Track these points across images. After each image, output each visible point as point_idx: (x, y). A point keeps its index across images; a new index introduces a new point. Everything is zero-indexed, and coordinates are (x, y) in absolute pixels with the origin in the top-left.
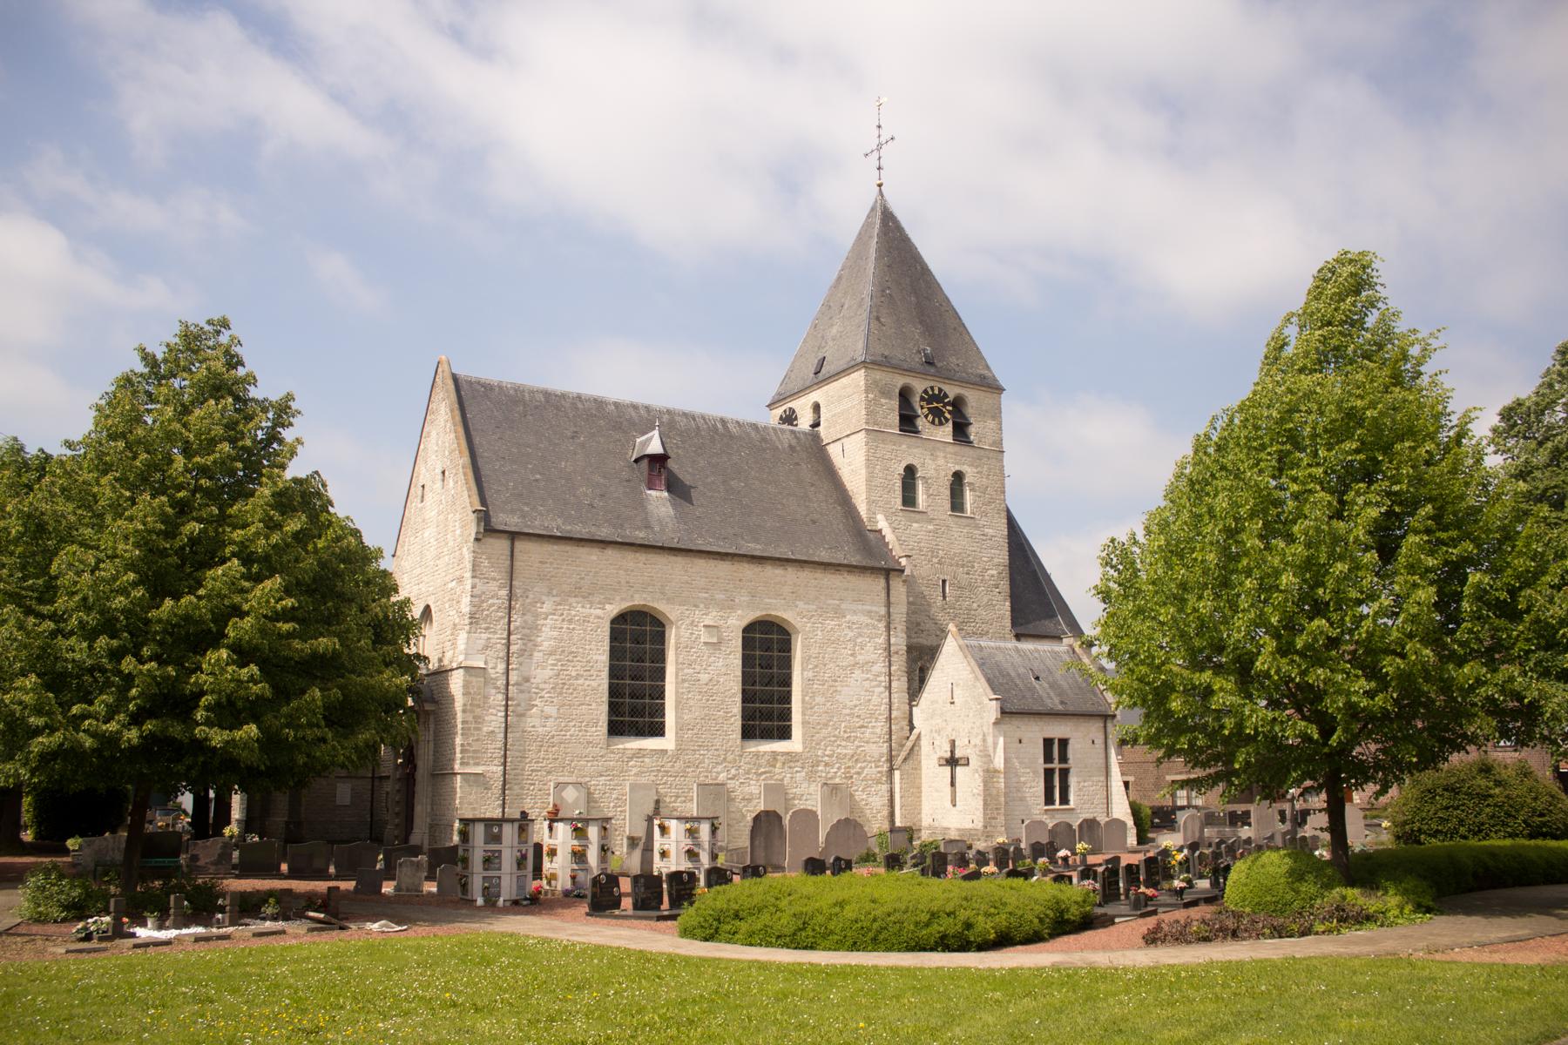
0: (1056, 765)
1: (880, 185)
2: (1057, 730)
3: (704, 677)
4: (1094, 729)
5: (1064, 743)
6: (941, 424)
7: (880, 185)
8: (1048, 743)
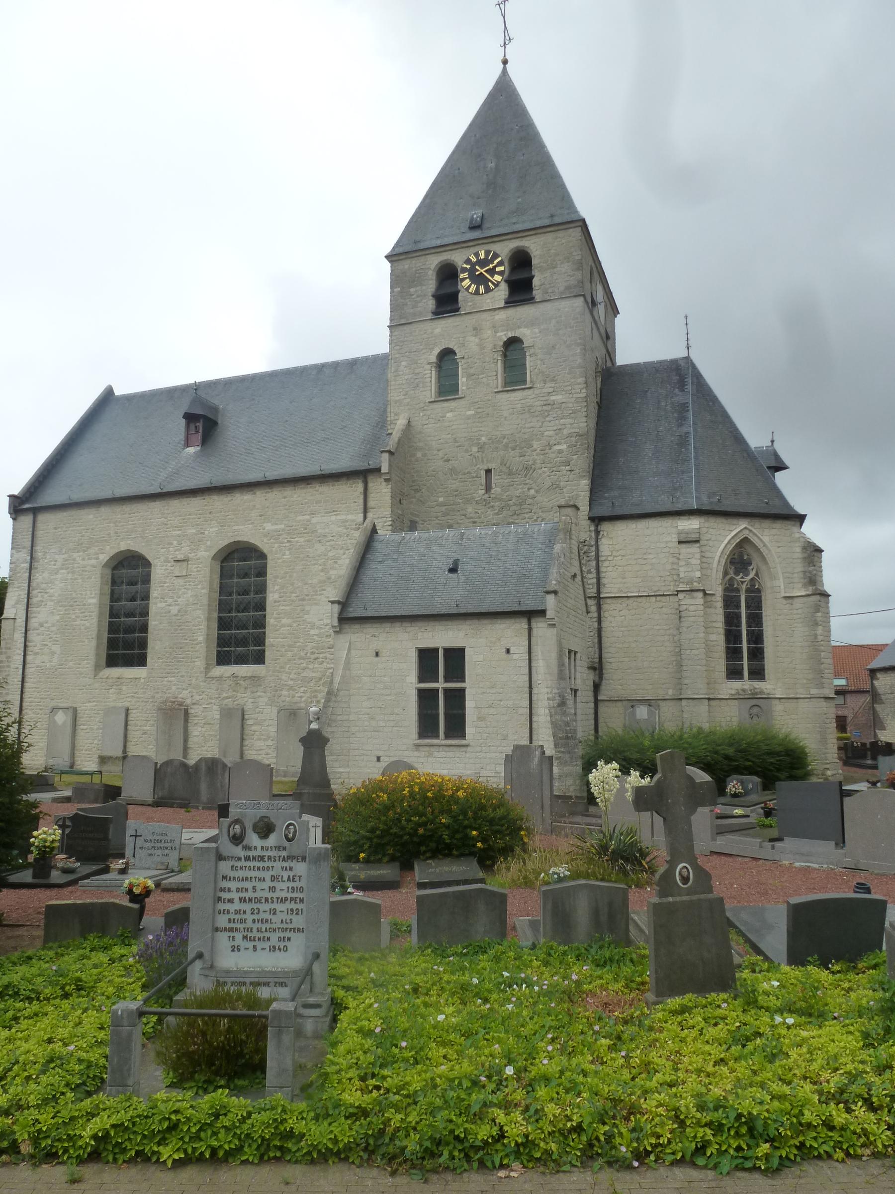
0: (441, 685)
1: (505, 62)
2: (442, 637)
3: (174, 610)
4: (511, 633)
5: (456, 658)
6: (488, 290)
7: (505, 62)
8: (427, 656)
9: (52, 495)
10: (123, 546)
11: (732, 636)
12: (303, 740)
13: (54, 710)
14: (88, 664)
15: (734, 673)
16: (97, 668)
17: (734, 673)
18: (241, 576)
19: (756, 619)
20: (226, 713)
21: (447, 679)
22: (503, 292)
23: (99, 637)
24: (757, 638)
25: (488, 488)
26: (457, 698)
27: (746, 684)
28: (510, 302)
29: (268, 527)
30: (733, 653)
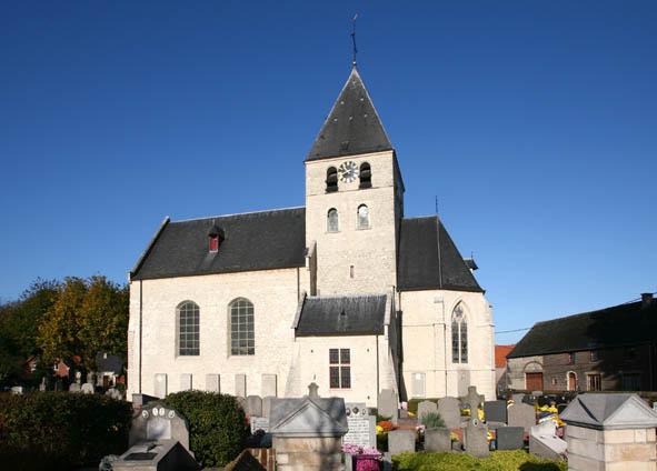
0: (340, 365)
5: (346, 354)
8: (333, 353)
9: (590, 420)
10: (185, 299)
11: (455, 344)
12: (309, 387)
13: (156, 375)
14: (225, 354)
15: (455, 360)
16: (176, 356)
17: (455, 360)
18: (242, 314)
19: (464, 336)
20: (237, 376)
21: (342, 362)
22: (357, 182)
23: (176, 341)
24: (464, 345)
25: (352, 276)
26: (347, 371)
27: (460, 365)
28: (361, 187)
29: (254, 291)
30: (455, 350)
